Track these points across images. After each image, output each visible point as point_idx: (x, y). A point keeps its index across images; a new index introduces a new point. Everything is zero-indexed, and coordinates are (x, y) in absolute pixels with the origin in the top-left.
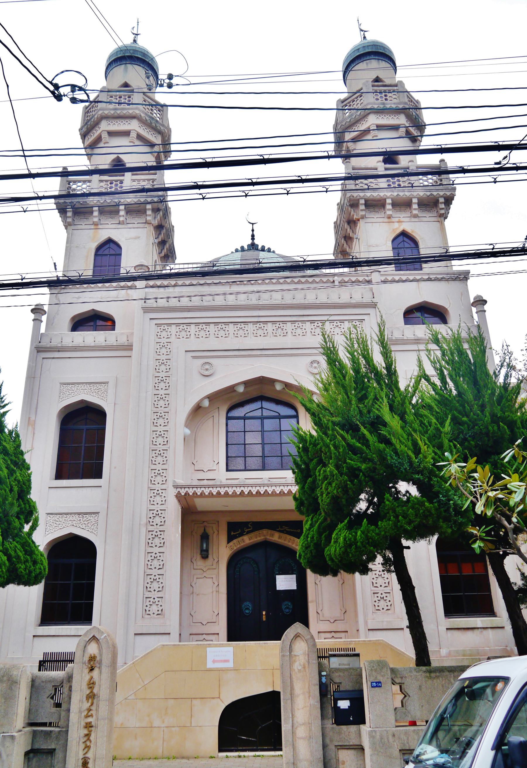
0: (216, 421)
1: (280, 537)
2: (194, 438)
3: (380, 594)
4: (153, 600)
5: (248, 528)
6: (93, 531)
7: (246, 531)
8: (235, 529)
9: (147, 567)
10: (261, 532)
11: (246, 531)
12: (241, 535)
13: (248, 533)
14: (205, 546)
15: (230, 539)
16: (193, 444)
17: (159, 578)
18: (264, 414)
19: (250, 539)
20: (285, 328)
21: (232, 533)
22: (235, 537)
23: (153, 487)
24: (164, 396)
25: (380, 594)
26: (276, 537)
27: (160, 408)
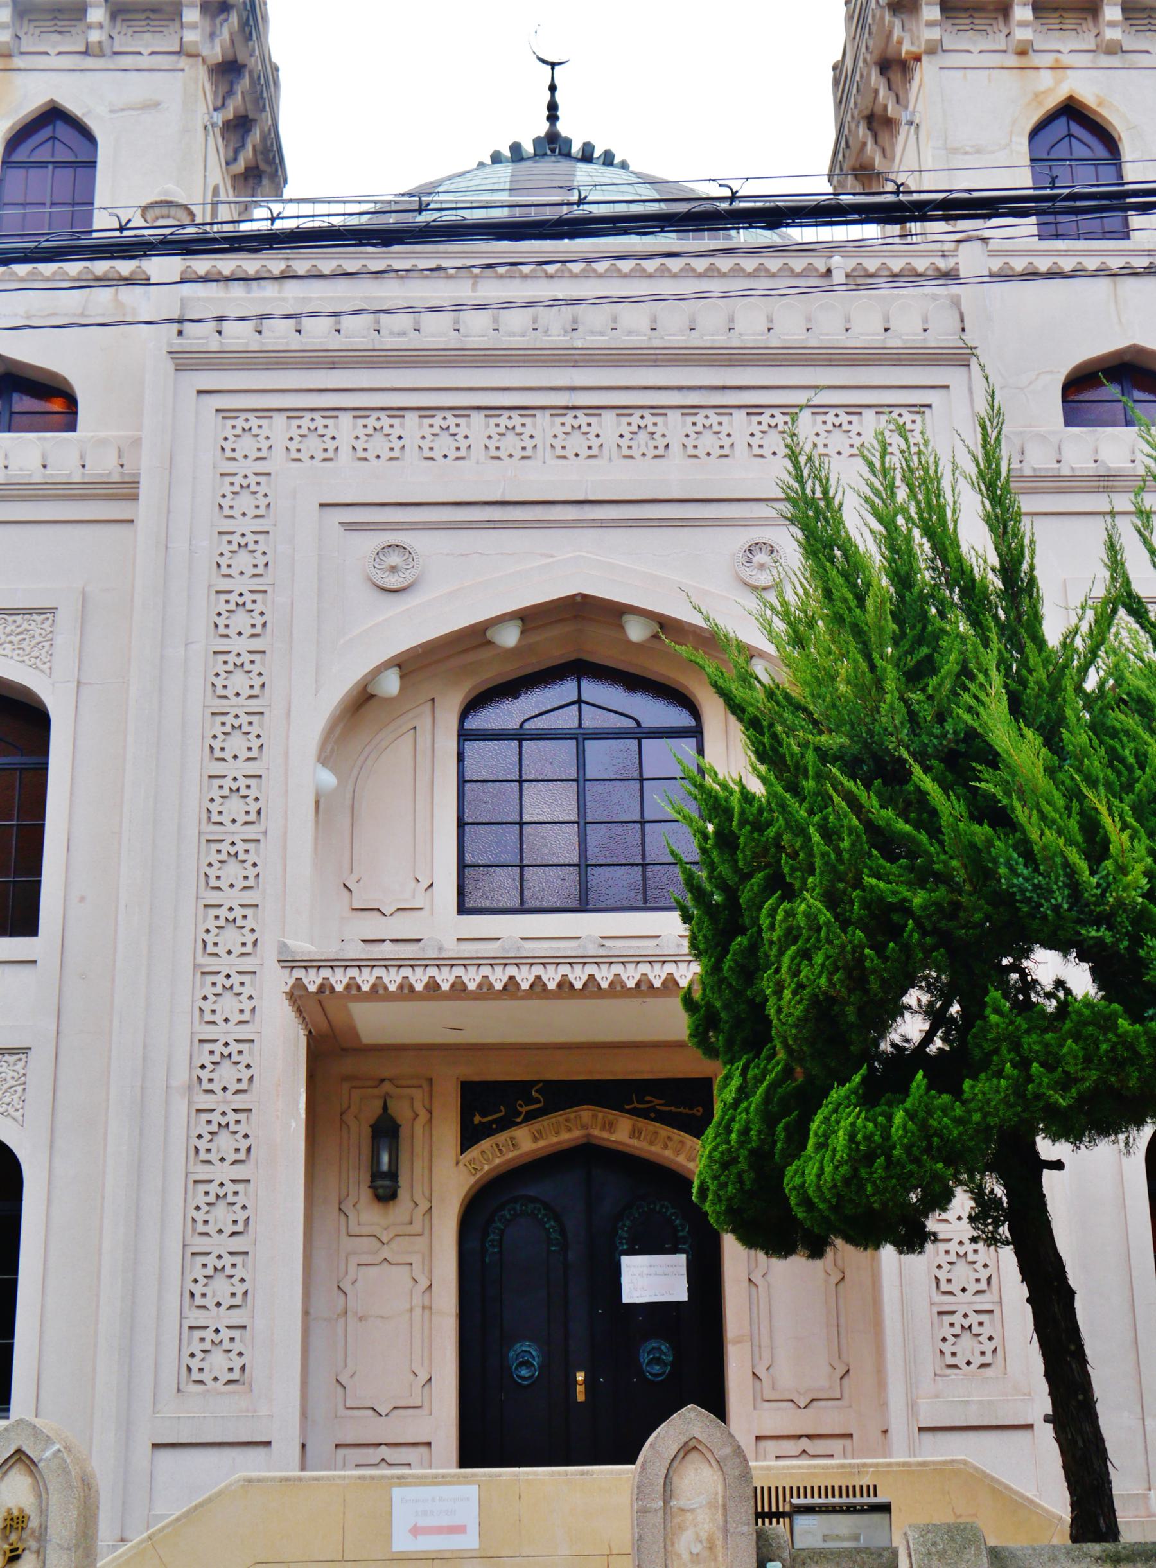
0: (424, 741)
1: (635, 1133)
2: (348, 802)
3: (959, 1315)
4: (214, 1336)
5: (530, 1101)
6: (11, 1111)
7: (524, 1109)
8: (487, 1105)
9: (207, 883)
10: (571, 1114)
11: (524, 1109)
12: (506, 1124)
13: (530, 1117)
14: (385, 1158)
15: (469, 1137)
16: (348, 820)
17: (245, 917)
18: (587, 723)
19: (535, 1139)
20: (659, 430)
21: (477, 1119)
22: (487, 1131)
23: (211, 964)
24: (246, 658)
25: (959, 1315)
26: (622, 1132)
27: (234, 700)
